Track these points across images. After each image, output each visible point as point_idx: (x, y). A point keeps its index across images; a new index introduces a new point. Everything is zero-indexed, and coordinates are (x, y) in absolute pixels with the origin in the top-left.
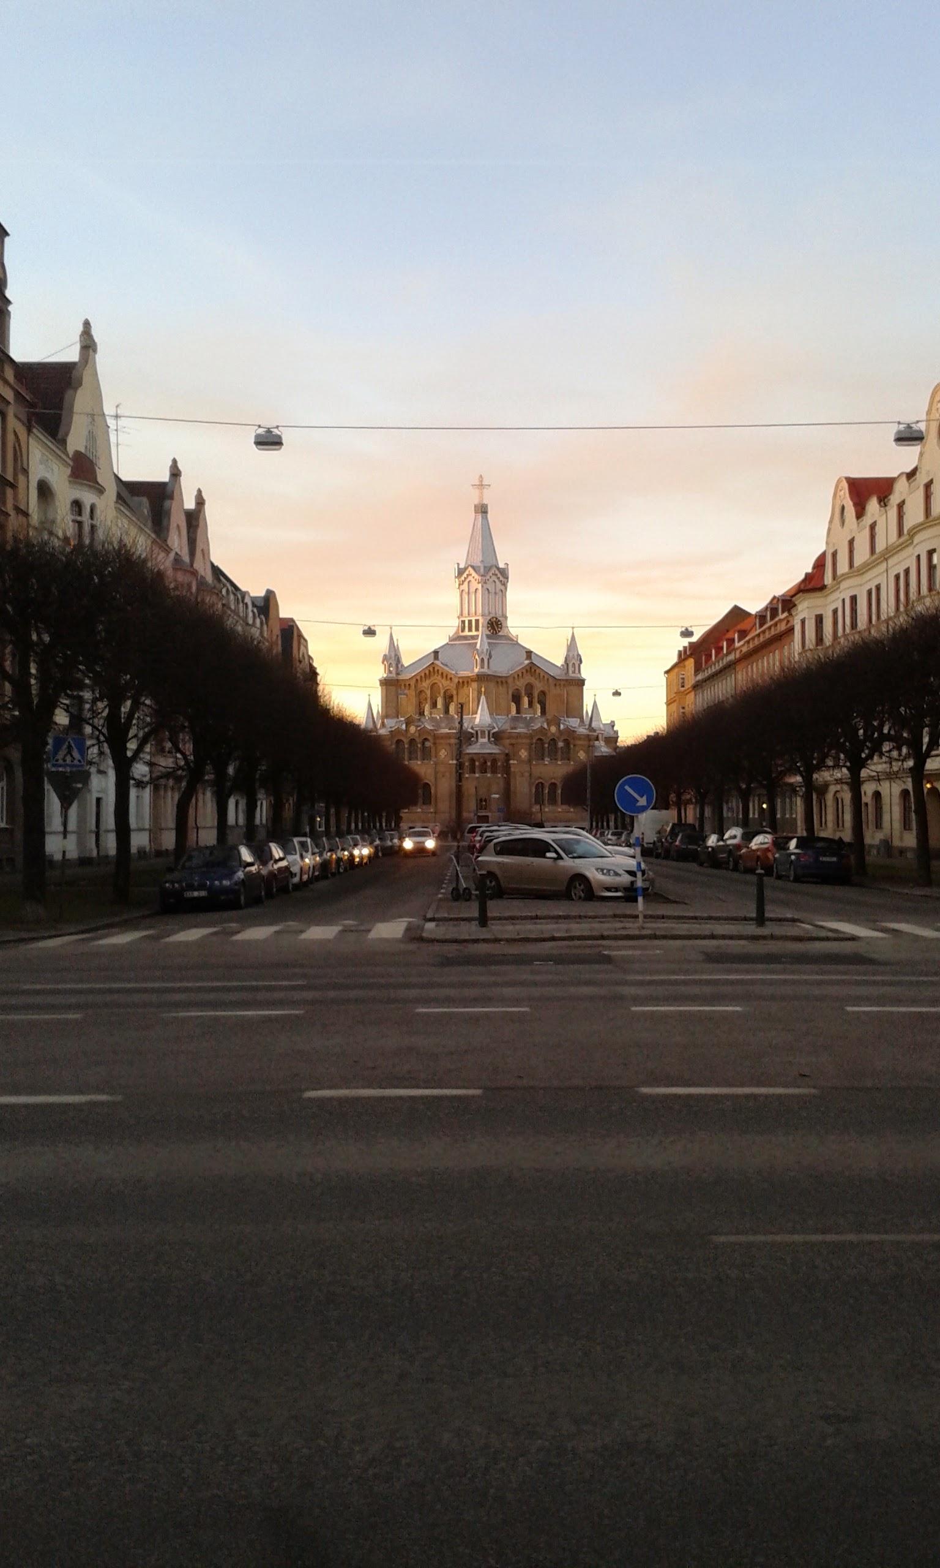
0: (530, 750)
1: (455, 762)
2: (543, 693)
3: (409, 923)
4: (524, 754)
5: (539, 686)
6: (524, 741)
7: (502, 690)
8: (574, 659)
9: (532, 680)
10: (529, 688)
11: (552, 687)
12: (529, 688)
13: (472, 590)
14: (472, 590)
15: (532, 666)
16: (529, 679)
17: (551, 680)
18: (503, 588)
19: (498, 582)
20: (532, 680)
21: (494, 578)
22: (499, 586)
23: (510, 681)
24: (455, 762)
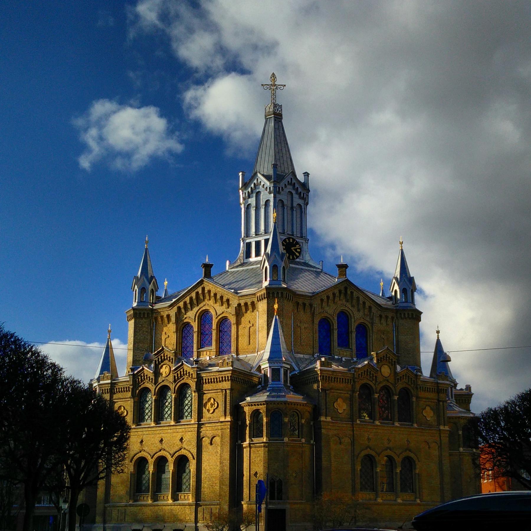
0: (351, 401)
1: (323, 418)
2: (362, 330)
3: (339, 345)
4: (342, 407)
5: (357, 318)
6: (341, 386)
7: (304, 316)
8: (407, 282)
9: (348, 307)
10: (344, 318)
11: (377, 320)
12: (344, 318)
13: (262, 202)
14: (262, 202)
15: (348, 290)
16: (342, 305)
17: (374, 310)
18: (301, 202)
19: (296, 196)
20: (348, 307)
21: (290, 188)
22: (297, 201)
23: (316, 303)
24: (323, 418)
